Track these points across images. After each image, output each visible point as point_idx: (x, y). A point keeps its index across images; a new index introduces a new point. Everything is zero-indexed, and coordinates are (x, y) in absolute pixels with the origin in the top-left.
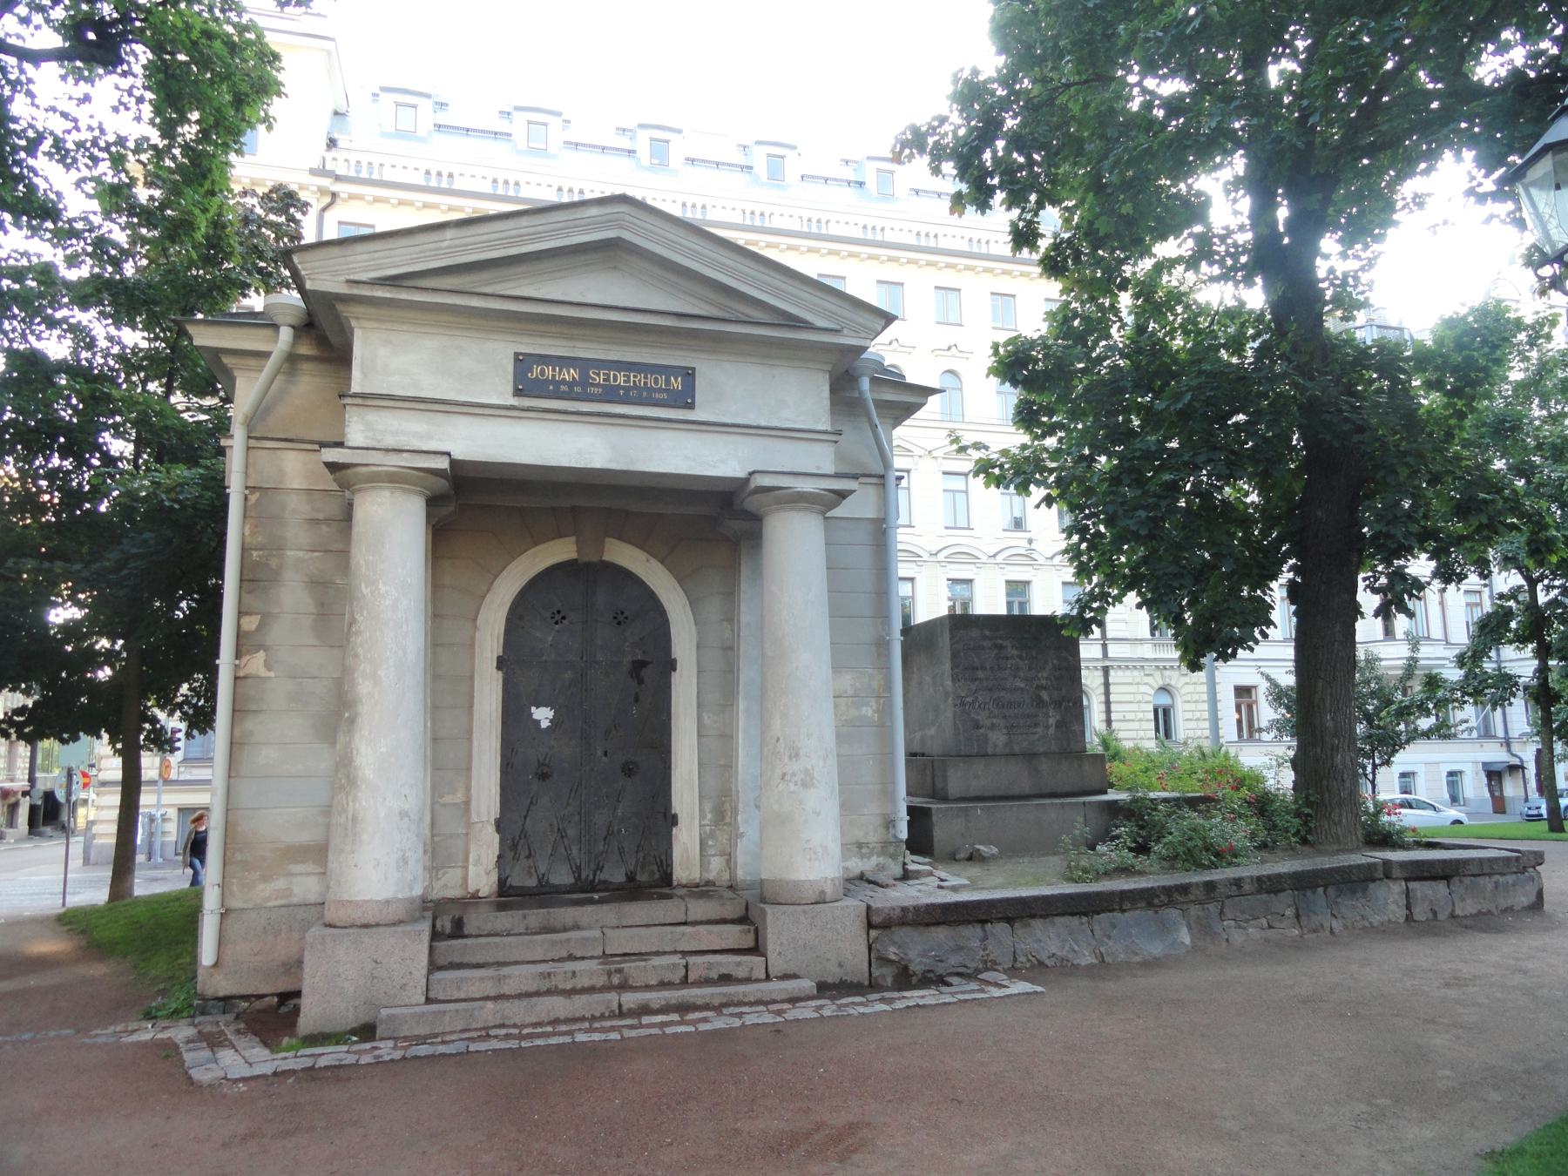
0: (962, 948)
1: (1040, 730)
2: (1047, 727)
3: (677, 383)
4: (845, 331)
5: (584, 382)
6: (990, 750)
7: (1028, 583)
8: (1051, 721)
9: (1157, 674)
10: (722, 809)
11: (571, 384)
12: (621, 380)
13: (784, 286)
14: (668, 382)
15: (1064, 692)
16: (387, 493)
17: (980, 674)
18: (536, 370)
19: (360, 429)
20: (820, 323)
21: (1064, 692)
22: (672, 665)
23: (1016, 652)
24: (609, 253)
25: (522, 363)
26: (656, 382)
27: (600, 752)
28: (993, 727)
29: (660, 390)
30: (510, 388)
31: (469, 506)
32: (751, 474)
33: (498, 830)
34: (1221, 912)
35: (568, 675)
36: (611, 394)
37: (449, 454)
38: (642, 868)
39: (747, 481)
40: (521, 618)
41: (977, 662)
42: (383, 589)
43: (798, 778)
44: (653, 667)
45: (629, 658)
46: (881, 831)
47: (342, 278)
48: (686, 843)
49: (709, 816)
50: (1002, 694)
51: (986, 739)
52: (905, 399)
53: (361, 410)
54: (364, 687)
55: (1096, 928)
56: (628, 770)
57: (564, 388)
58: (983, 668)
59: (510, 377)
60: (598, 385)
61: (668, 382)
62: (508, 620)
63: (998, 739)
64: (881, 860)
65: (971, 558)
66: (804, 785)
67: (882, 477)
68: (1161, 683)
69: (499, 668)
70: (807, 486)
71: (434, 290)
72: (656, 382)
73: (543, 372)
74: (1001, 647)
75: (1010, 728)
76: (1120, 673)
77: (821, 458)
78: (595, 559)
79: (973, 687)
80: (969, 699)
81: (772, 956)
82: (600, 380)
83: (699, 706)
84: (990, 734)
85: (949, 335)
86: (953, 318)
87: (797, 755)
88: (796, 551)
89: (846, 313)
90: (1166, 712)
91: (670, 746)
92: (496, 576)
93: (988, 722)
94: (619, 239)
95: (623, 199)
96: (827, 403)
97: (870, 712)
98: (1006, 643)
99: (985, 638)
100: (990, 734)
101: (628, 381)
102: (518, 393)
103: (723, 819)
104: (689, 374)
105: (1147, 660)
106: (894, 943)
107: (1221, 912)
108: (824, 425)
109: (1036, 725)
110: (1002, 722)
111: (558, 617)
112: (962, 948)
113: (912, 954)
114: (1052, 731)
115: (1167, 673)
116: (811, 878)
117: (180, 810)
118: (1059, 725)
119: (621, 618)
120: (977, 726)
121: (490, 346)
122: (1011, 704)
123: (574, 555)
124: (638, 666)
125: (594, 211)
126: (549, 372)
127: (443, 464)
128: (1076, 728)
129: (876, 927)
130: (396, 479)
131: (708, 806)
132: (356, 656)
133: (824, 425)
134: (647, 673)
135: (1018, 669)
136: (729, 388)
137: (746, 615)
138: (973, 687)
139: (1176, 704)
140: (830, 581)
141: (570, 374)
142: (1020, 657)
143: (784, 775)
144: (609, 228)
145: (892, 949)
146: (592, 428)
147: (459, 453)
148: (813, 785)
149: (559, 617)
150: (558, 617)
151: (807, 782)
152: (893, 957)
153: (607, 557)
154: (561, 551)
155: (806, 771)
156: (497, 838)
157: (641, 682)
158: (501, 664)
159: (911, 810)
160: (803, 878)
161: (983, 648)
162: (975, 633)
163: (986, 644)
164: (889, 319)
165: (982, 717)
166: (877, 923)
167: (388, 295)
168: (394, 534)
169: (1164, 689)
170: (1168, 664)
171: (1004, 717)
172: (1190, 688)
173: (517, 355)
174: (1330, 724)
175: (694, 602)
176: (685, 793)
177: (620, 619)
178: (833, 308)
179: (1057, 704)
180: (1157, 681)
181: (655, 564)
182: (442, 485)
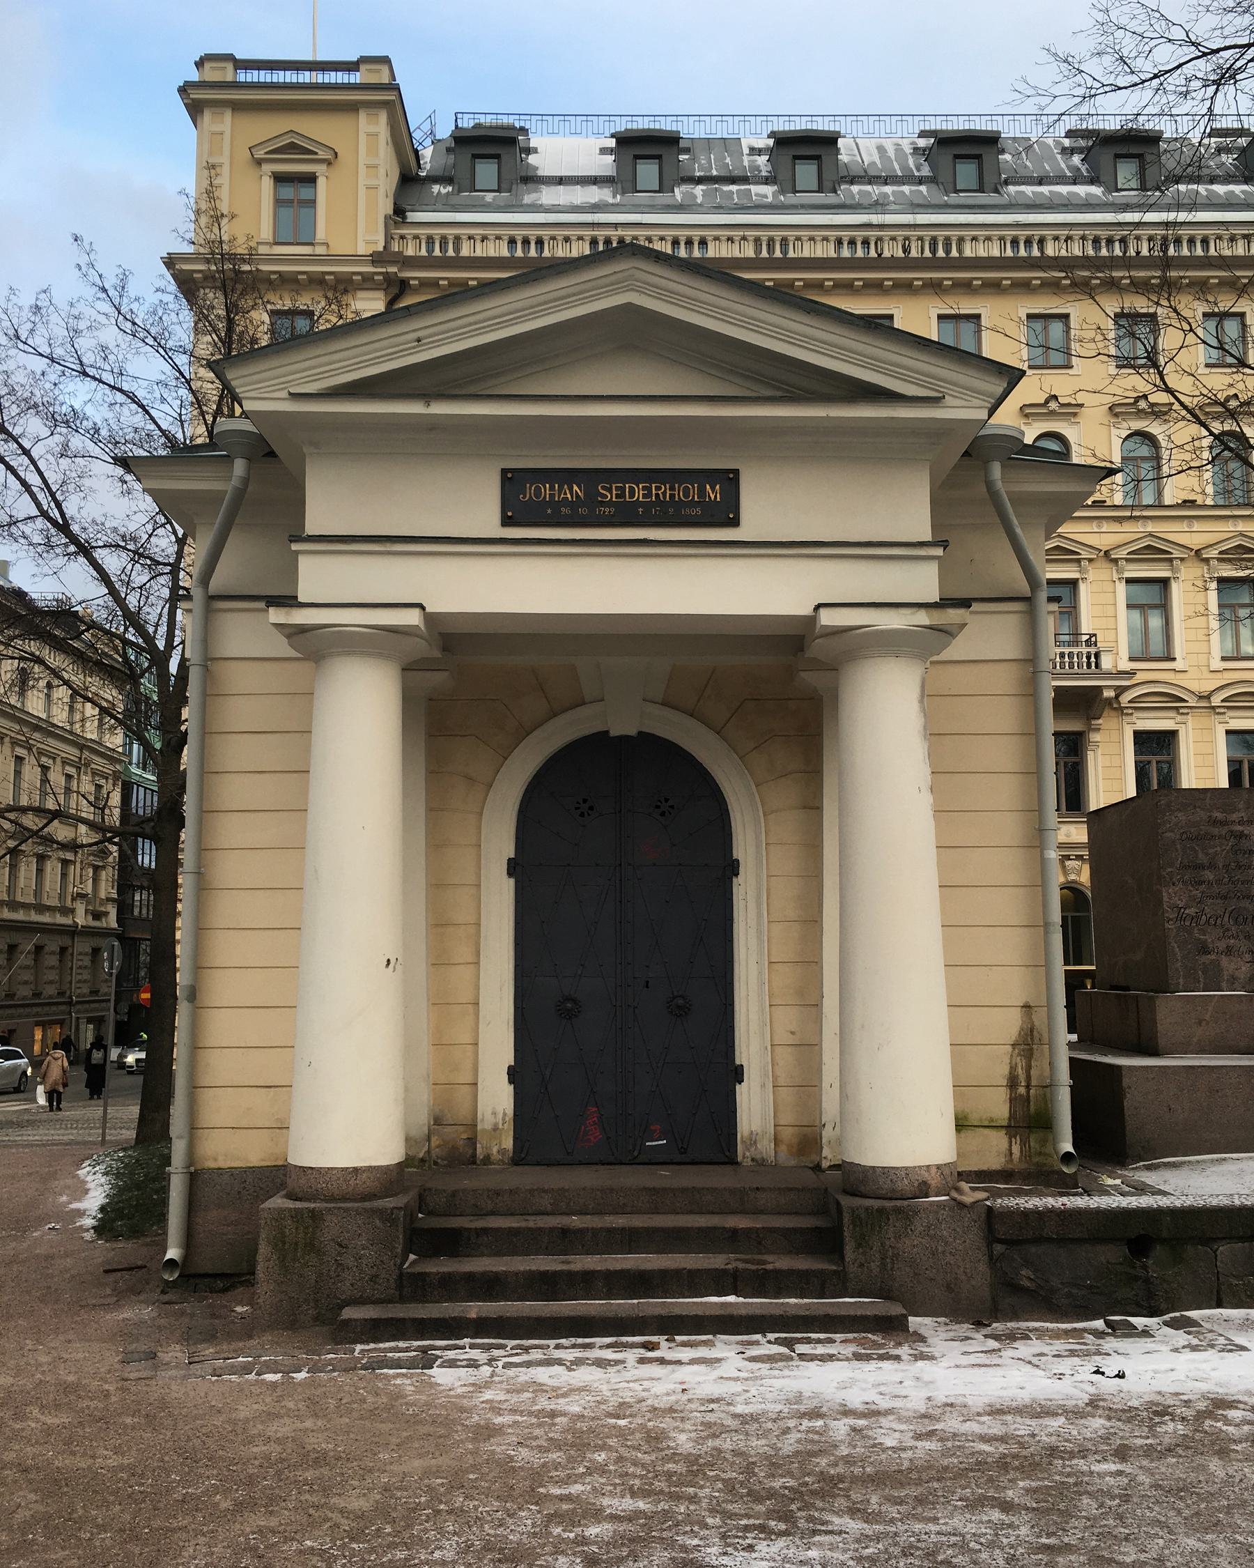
3: (714, 493)
5: (592, 499)
11: (573, 505)
12: (639, 494)
14: (702, 492)
17: (1209, 875)
18: (530, 490)
19: (319, 577)
25: (511, 481)
26: (686, 494)
28: (1229, 951)
31: (463, 688)
36: (627, 516)
37: (421, 606)
39: (811, 621)
41: (1202, 858)
58: (1212, 866)
65: (1173, 702)
72: (686, 494)
73: (538, 490)
80: (1191, 911)
82: (611, 496)
84: (1224, 961)
91: (516, 1050)
93: (1222, 945)
94: (629, 308)
100: (1224, 961)
101: (649, 495)
102: (507, 521)
120: (1204, 950)
127: (412, 618)
129: (1000, 1241)
137: (424, 1097)
138: (1197, 893)
140: (933, 755)
144: (615, 292)
147: (436, 606)
163: (1216, 831)
168: (362, 720)
173: (504, 472)
182: (421, 648)
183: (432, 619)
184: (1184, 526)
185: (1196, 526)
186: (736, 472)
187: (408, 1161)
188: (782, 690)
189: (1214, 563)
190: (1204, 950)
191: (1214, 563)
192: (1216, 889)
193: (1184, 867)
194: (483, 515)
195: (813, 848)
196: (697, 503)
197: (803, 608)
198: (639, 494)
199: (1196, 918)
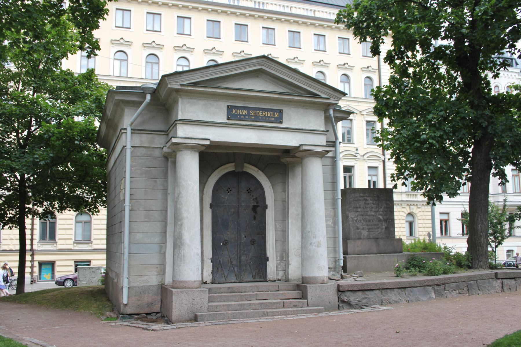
0: (366, 298)
1: (379, 230)
2: (382, 229)
4: (331, 99)
5: (249, 115)
6: (362, 237)
7: (353, 166)
8: (384, 227)
9: (408, 207)
10: (284, 257)
11: (245, 116)
12: (260, 114)
13: (312, 84)
14: (274, 114)
15: (388, 216)
16: (189, 152)
17: (359, 210)
18: (234, 111)
19: (183, 132)
20: (323, 96)
21: (388, 216)
22: (266, 207)
23: (371, 202)
24: (258, 73)
26: (271, 114)
27: (243, 236)
28: (363, 229)
29: (272, 117)
30: (226, 117)
31: (211, 157)
32: (300, 145)
33: (212, 262)
34: (445, 288)
35: (233, 210)
38: (258, 274)
39: (299, 147)
40: (217, 190)
41: (358, 205)
42: (190, 183)
43: (316, 244)
44: (259, 208)
45: (252, 204)
46: (334, 263)
47: (179, 84)
48: (271, 267)
49: (278, 258)
50: (367, 217)
51: (361, 233)
52: (345, 115)
53: (182, 125)
54: (185, 214)
55: (406, 293)
56: (253, 242)
57: (242, 117)
58: (360, 207)
59: (226, 113)
60: (253, 116)
61: (274, 114)
62: (213, 191)
63: (365, 233)
64: (334, 273)
66: (318, 246)
67: (334, 142)
68: (409, 211)
69: (210, 208)
70: (319, 149)
71: (206, 87)
72: (271, 114)
73: (236, 112)
74: (366, 200)
75: (369, 229)
76: (398, 207)
77: (322, 140)
78: (241, 171)
79: (357, 214)
80: (355, 219)
81: (309, 300)
83: (275, 221)
85: (320, 56)
86: (322, 48)
87: (315, 237)
88: (316, 170)
89: (331, 93)
90: (446, 221)
92: (209, 176)
93: (362, 227)
94: (261, 69)
95: (264, 57)
96: (323, 121)
97: (330, 223)
98: (368, 198)
99: (361, 196)
102: (228, 119)
103: (283, 259)
104: (281, 112)
105: (403, 201)
106: (346, 296)
107: (445, 288)
108: (322, 128)
109: (378, 228)
110: (366, 227)
111: (229, 190)
112: (366, 298)
113: (351, 300)
114: (384, 230)
115: (411, 207)
116: (320, 276)
117: (75, 262)
118: (386, 228)
119: (249, 191)
120: (358, 229)
121: (220, 103)
122: (369, 221)
123: (234, 169)
124: (255, 208)
125: (254, 61)
126: (238, 112)
127: (208, 143)
128: (392, 229)
130: (192, 148)
131: (278, 254)
132: (182, 204)
133: (322, 128)
134: (258, 209)
135: (372, 208)
136: (293, 118)
139: (431, 220)
141: (244, 112)
142: (373, 203)
143: (311, 243)
144: (258, 66)
145: (345, 298)
146: (251, 130)
148: (320, 247)
149: (229, 190)
150: (229, 190)
151: (319, 246)
152: (346, 300)
153: (244, 170)
154: (229, 168)
155: (318, 242)
156: (211, 264)
157: (256, 213)
158: (211, 206)
159: (344, 257)
160: (318, 276)
161: (360, 200)
162: (357, 195)
163: (361, 199)
164: (344, 94)
165: (359, 225)
166: (340, 290)
167: (192, 89)
168: (189, 166)
169: (410, 214)
170: (412, 203)
171: (367, 225)
172: (421, 214)
173: (228, 106)
174: (479, 228)
175: (273, 185)
176: (271, 250)
177: (249, 191)
178: (327, 91)
179: (386, 221)
180: (407, 210)
181: (260, 172)
183: (211, 141)
184: (356, 104)
185: (360, 104)
186: (282, 110)
187: (488, 200)
188: (282, 162)
189: (365, 115)
190: (358, 229)
191: (365, 115)
192: (361, 213)
193: (354, 208)
194: (223, 119)
195: (166, 194)
196: (274, 118)
197: (297, 145)
198: (260, 114)
199: (357, 220)
